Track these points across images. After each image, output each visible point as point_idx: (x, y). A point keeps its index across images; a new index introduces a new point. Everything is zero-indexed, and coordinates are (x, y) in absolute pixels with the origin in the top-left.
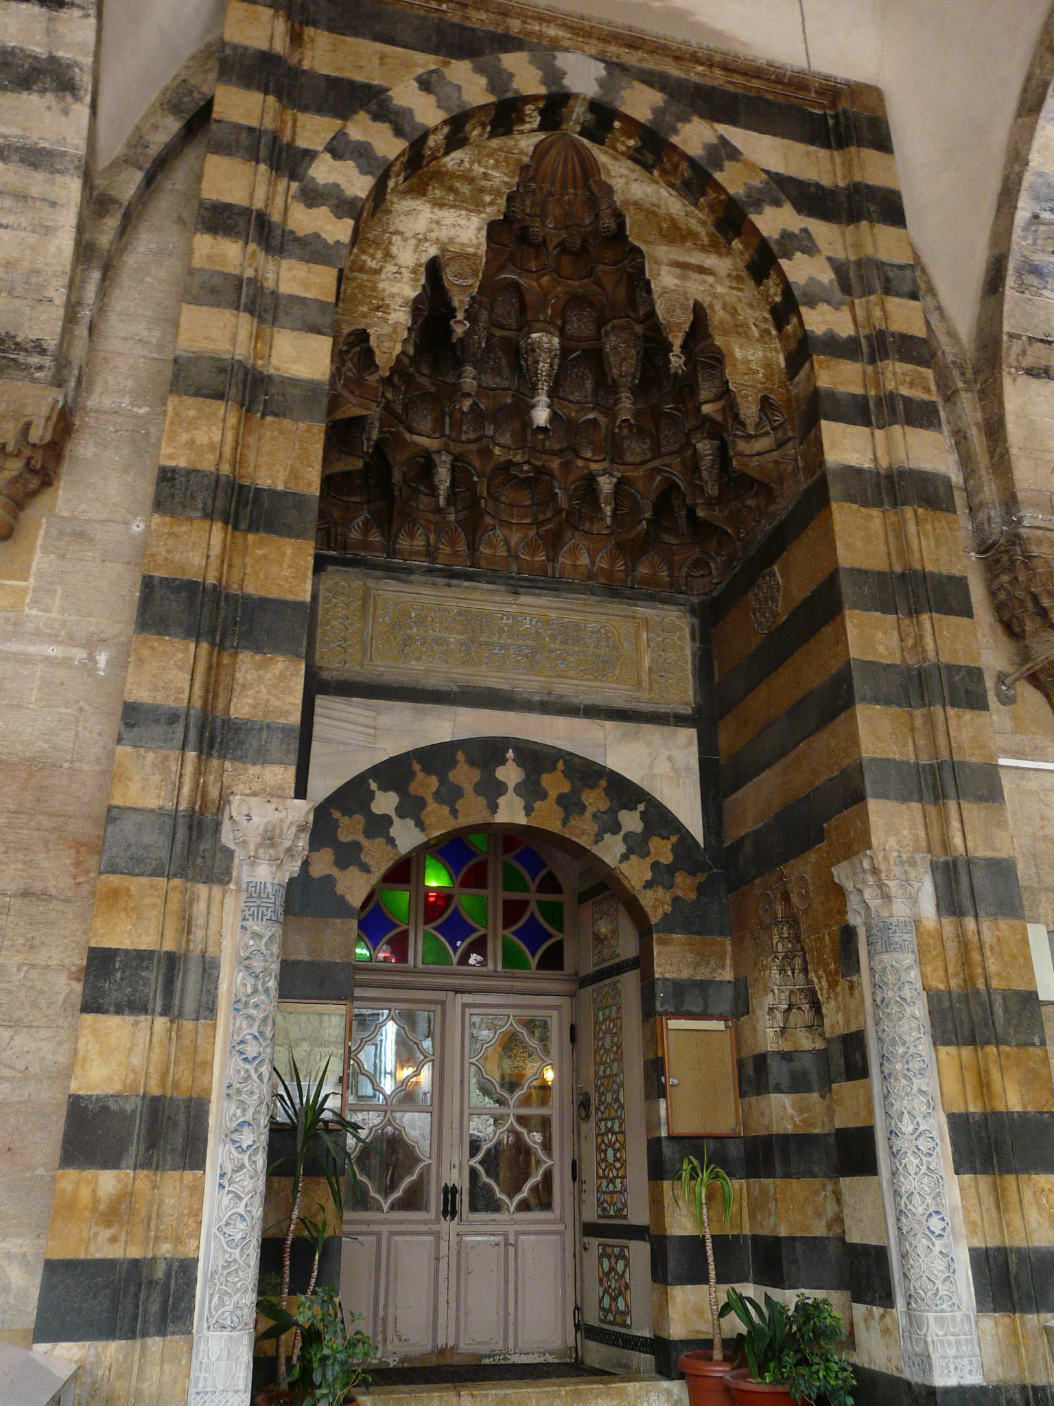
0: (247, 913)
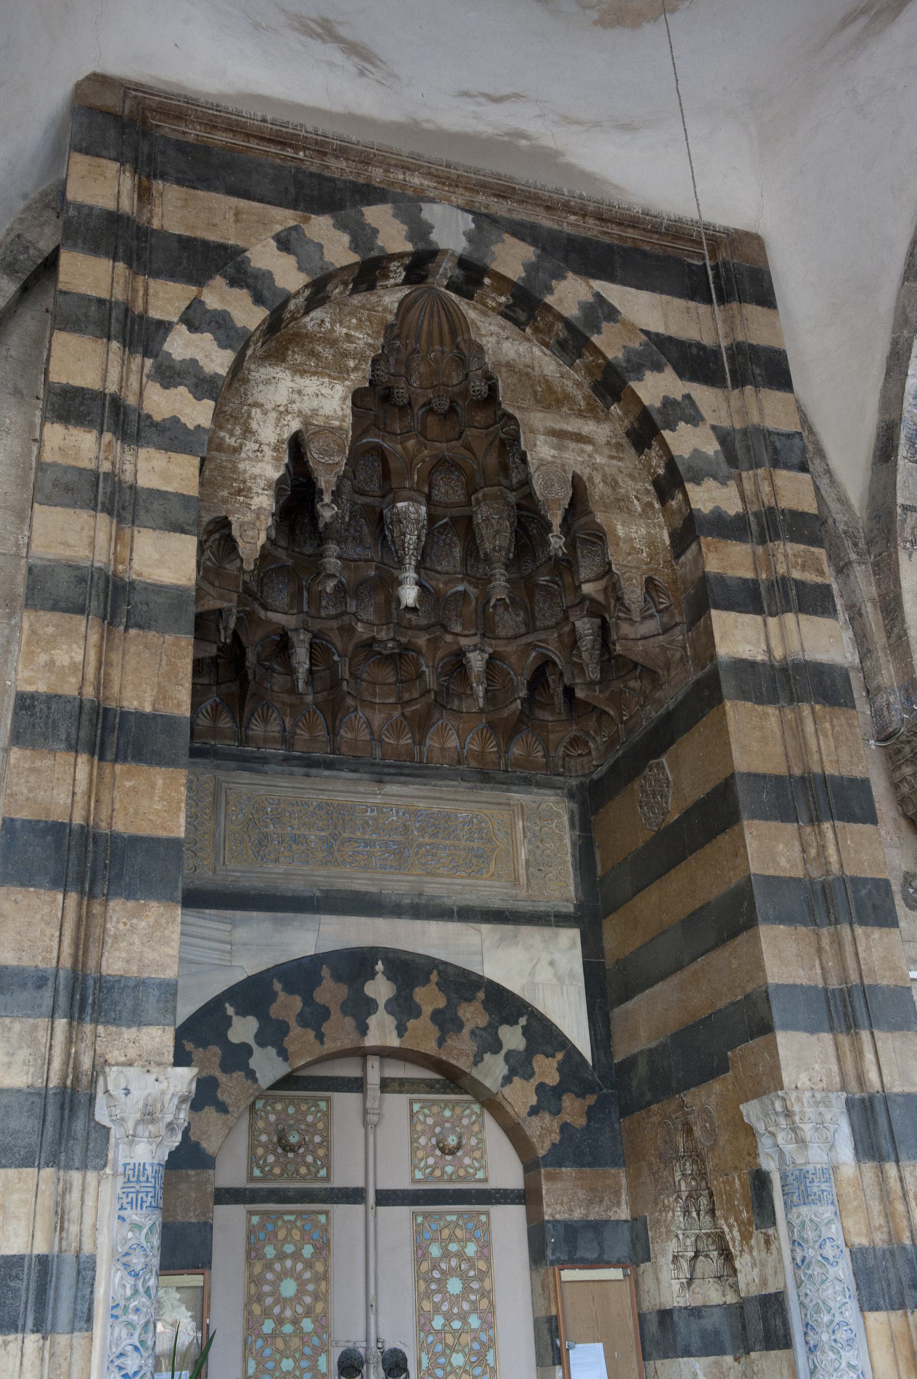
0: (125, 1201)
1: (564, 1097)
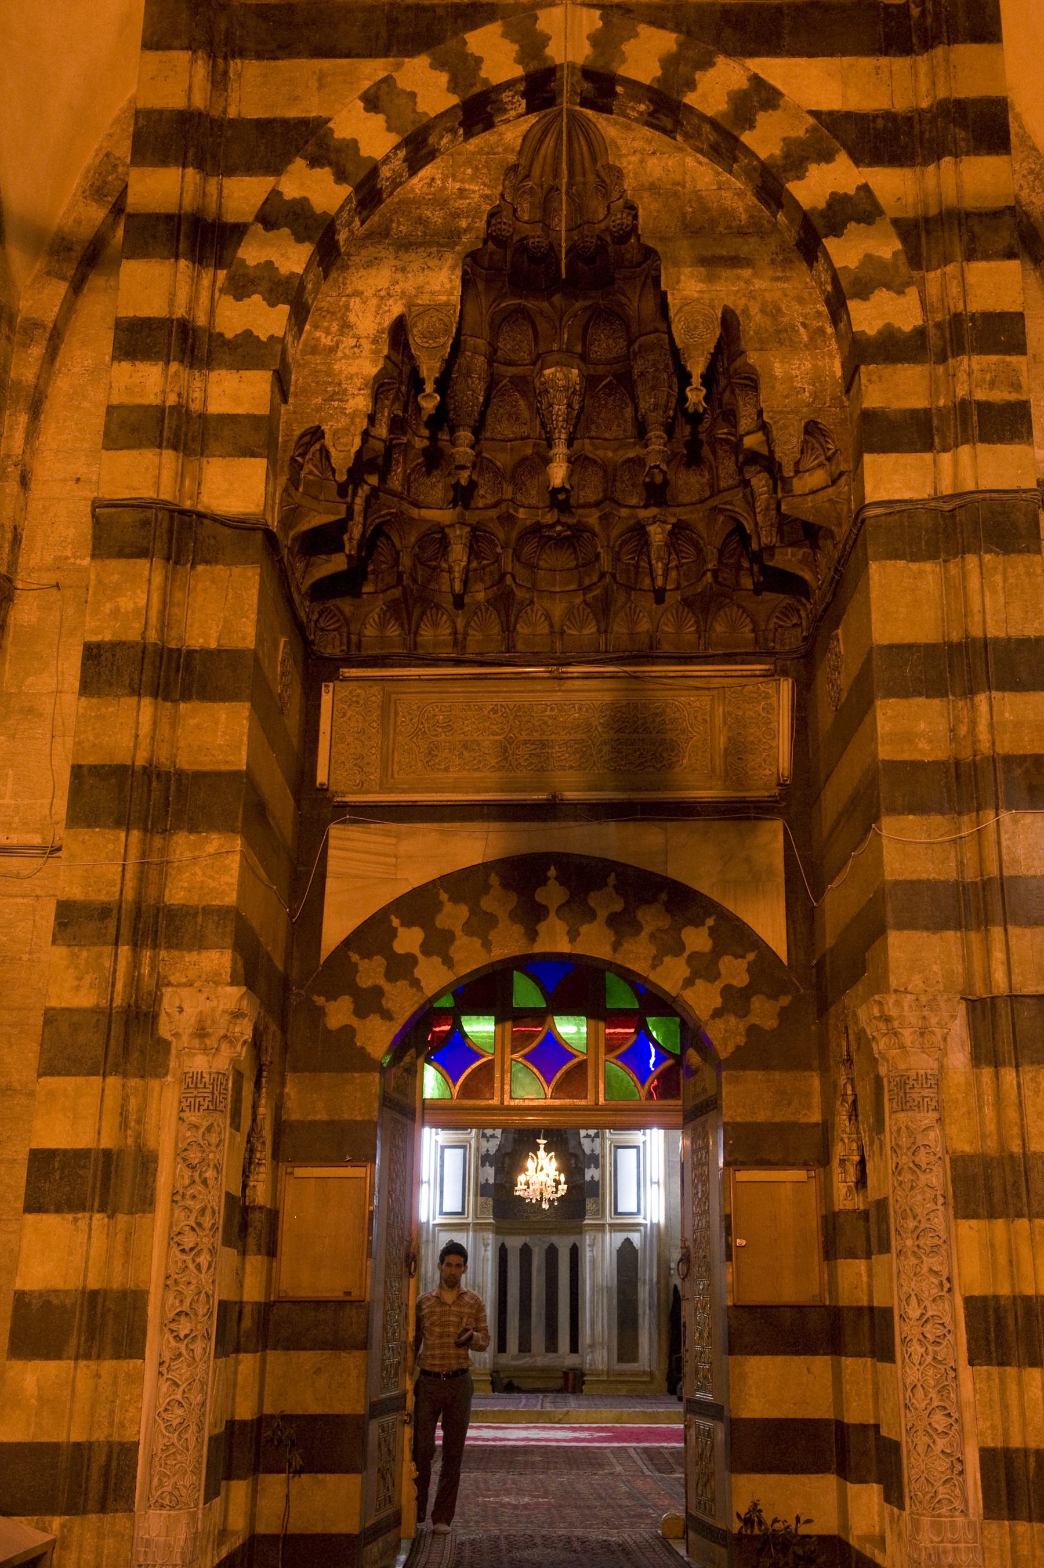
0: (184, 1104)
1: (753, 999)
